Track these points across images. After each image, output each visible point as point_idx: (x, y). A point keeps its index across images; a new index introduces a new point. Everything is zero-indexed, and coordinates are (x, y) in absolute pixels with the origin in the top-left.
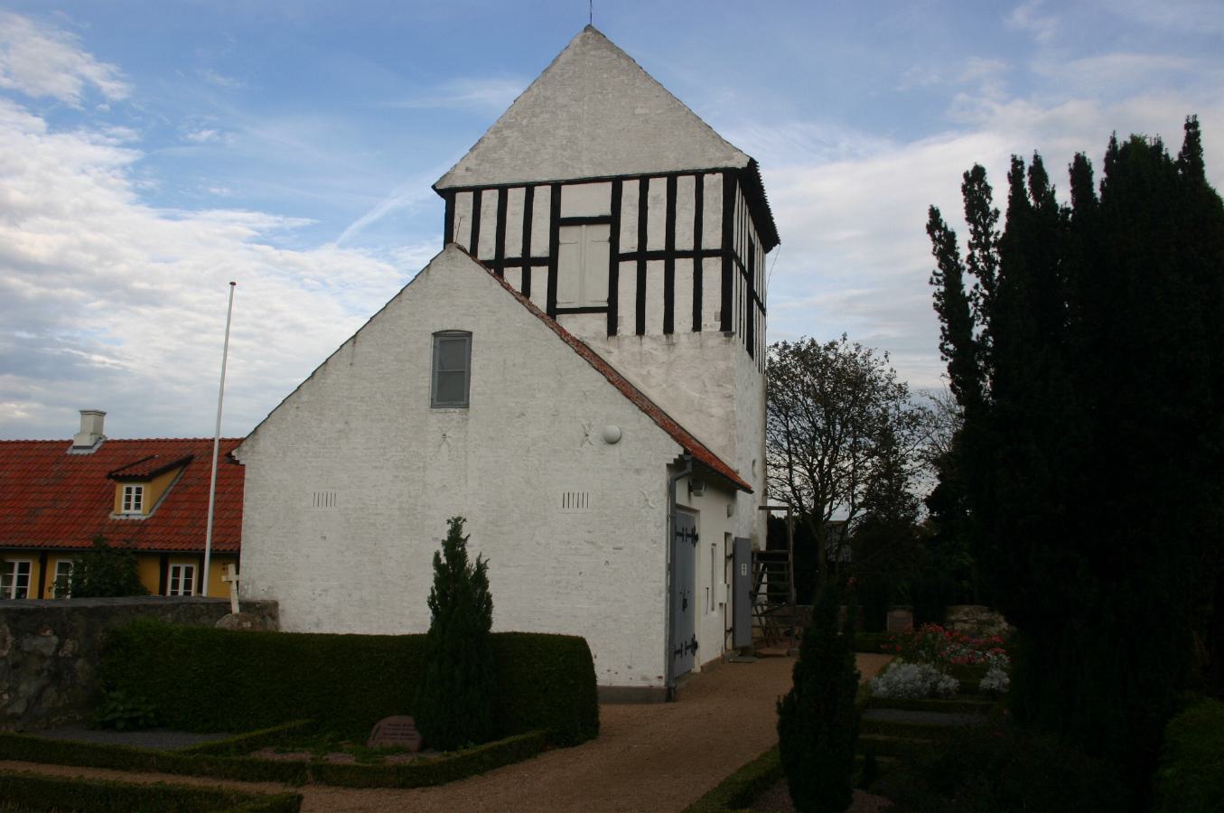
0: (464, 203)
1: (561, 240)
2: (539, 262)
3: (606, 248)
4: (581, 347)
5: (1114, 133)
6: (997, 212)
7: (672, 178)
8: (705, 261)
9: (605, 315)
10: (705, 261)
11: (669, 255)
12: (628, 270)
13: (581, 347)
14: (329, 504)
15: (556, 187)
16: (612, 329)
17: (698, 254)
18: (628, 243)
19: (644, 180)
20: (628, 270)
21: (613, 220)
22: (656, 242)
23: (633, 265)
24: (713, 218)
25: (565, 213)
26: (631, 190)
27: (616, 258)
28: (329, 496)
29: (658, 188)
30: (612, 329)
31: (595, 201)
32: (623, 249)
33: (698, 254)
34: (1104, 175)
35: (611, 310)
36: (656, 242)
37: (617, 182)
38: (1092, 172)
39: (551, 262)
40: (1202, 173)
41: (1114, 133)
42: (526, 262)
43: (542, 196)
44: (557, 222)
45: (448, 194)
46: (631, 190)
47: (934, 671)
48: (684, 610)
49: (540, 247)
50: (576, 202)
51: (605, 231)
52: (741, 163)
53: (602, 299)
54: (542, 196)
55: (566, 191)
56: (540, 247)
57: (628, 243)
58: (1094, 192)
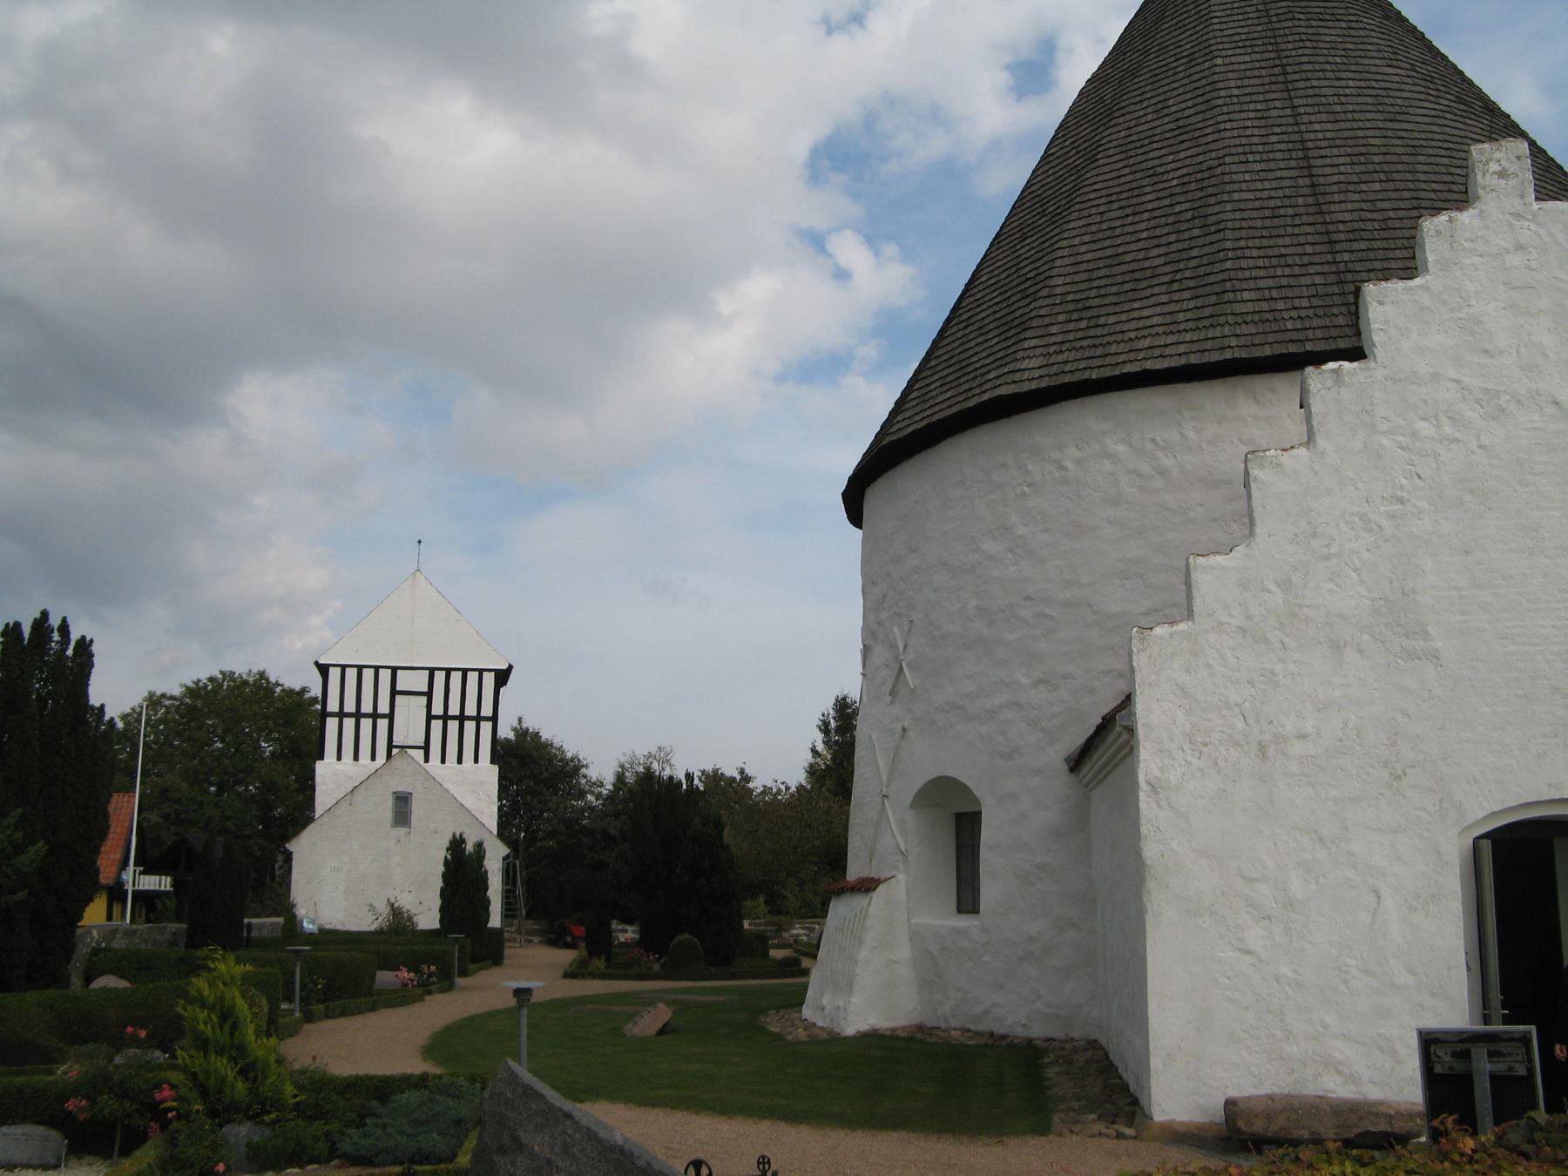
1: (396, 703)
2: (383, 716)
3: (424, 712)
8: (337, 710)
9: (422, 751)
10: (337, 710)
11: (358, 715)
12: (437, 726)
16: (427, 760)
18: (438, 709)
20: (437, 726)
21: (429, 694)
22: (454, 709)
23: (347, 710)
26: (440, 677)
27: (430, 717)
29: (456, 678)
32: (490, 724)
34: (504, 850)
35: (426, 748)
36: (454, 709)
37: (432, 671)
38: (486, 872)
39: (391, 717)
40: (87, 905)
43: (385, 676)
44: (394, 692)
46: (440, 677)
49: (384, 708)
51: (424, 700)
53: (421, 742)
56: (384, 708)
57: (438, 709)
58: (1330, 363)
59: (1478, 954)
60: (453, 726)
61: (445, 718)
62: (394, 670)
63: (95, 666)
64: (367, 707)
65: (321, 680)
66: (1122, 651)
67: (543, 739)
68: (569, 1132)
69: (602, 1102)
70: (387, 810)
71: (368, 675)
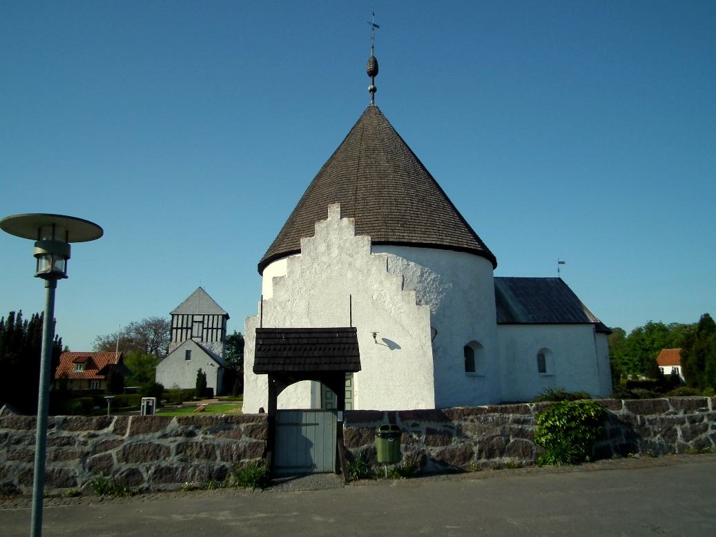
0: (176, 317)
4: (197, 344)
5: (21, 311)
6: (258, 370)
7: (213, 315)
11: (212, 328)
12: (205, 331)
13: (197, 344)
14: (209, 340)
15: (193, 316)
16: (202, 340)
17: (217, 329)
18: (205, 326)
19: (213, 315)
20: (205, 331)
21: (203, 322)
24: (220, 323)
25: (194, 320)
26: (206, 317)
27: (203, 328)
28: (209, 340)
29: (211, 317)
30: (202, 340)
31: (200, 318)
33: (217, 329)
35: (202, 337)
37: (204, 315)
39: (191, 329)
41: (21, 311)
42: (187, 328)
43: (190, 317)
44: (193, 321)
45: (173, 315)
46: (206, 317)
47: (259, 469)
48: (375, 63)
49: (190, 326)
50: (197, 318)
52: (225, 313)
54: (190, 317)
55: (195, 317)
56: (190, 326)
59: (414, 248)
60: (210, 331)
61: (208, 328)
62: (193, 316)
63: (619, 327)
64: (215, 326)
65: (55, 316)
66: (482, 418)
67: (628, 332)
68: (556, 413)
69: (291, 485)
70: (184, 356)
71: (185, 316)
